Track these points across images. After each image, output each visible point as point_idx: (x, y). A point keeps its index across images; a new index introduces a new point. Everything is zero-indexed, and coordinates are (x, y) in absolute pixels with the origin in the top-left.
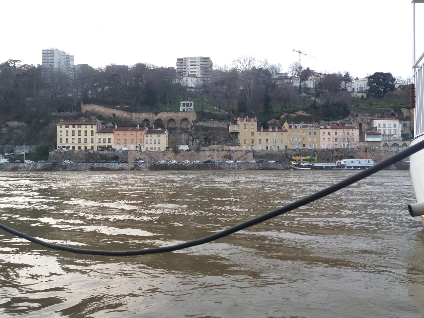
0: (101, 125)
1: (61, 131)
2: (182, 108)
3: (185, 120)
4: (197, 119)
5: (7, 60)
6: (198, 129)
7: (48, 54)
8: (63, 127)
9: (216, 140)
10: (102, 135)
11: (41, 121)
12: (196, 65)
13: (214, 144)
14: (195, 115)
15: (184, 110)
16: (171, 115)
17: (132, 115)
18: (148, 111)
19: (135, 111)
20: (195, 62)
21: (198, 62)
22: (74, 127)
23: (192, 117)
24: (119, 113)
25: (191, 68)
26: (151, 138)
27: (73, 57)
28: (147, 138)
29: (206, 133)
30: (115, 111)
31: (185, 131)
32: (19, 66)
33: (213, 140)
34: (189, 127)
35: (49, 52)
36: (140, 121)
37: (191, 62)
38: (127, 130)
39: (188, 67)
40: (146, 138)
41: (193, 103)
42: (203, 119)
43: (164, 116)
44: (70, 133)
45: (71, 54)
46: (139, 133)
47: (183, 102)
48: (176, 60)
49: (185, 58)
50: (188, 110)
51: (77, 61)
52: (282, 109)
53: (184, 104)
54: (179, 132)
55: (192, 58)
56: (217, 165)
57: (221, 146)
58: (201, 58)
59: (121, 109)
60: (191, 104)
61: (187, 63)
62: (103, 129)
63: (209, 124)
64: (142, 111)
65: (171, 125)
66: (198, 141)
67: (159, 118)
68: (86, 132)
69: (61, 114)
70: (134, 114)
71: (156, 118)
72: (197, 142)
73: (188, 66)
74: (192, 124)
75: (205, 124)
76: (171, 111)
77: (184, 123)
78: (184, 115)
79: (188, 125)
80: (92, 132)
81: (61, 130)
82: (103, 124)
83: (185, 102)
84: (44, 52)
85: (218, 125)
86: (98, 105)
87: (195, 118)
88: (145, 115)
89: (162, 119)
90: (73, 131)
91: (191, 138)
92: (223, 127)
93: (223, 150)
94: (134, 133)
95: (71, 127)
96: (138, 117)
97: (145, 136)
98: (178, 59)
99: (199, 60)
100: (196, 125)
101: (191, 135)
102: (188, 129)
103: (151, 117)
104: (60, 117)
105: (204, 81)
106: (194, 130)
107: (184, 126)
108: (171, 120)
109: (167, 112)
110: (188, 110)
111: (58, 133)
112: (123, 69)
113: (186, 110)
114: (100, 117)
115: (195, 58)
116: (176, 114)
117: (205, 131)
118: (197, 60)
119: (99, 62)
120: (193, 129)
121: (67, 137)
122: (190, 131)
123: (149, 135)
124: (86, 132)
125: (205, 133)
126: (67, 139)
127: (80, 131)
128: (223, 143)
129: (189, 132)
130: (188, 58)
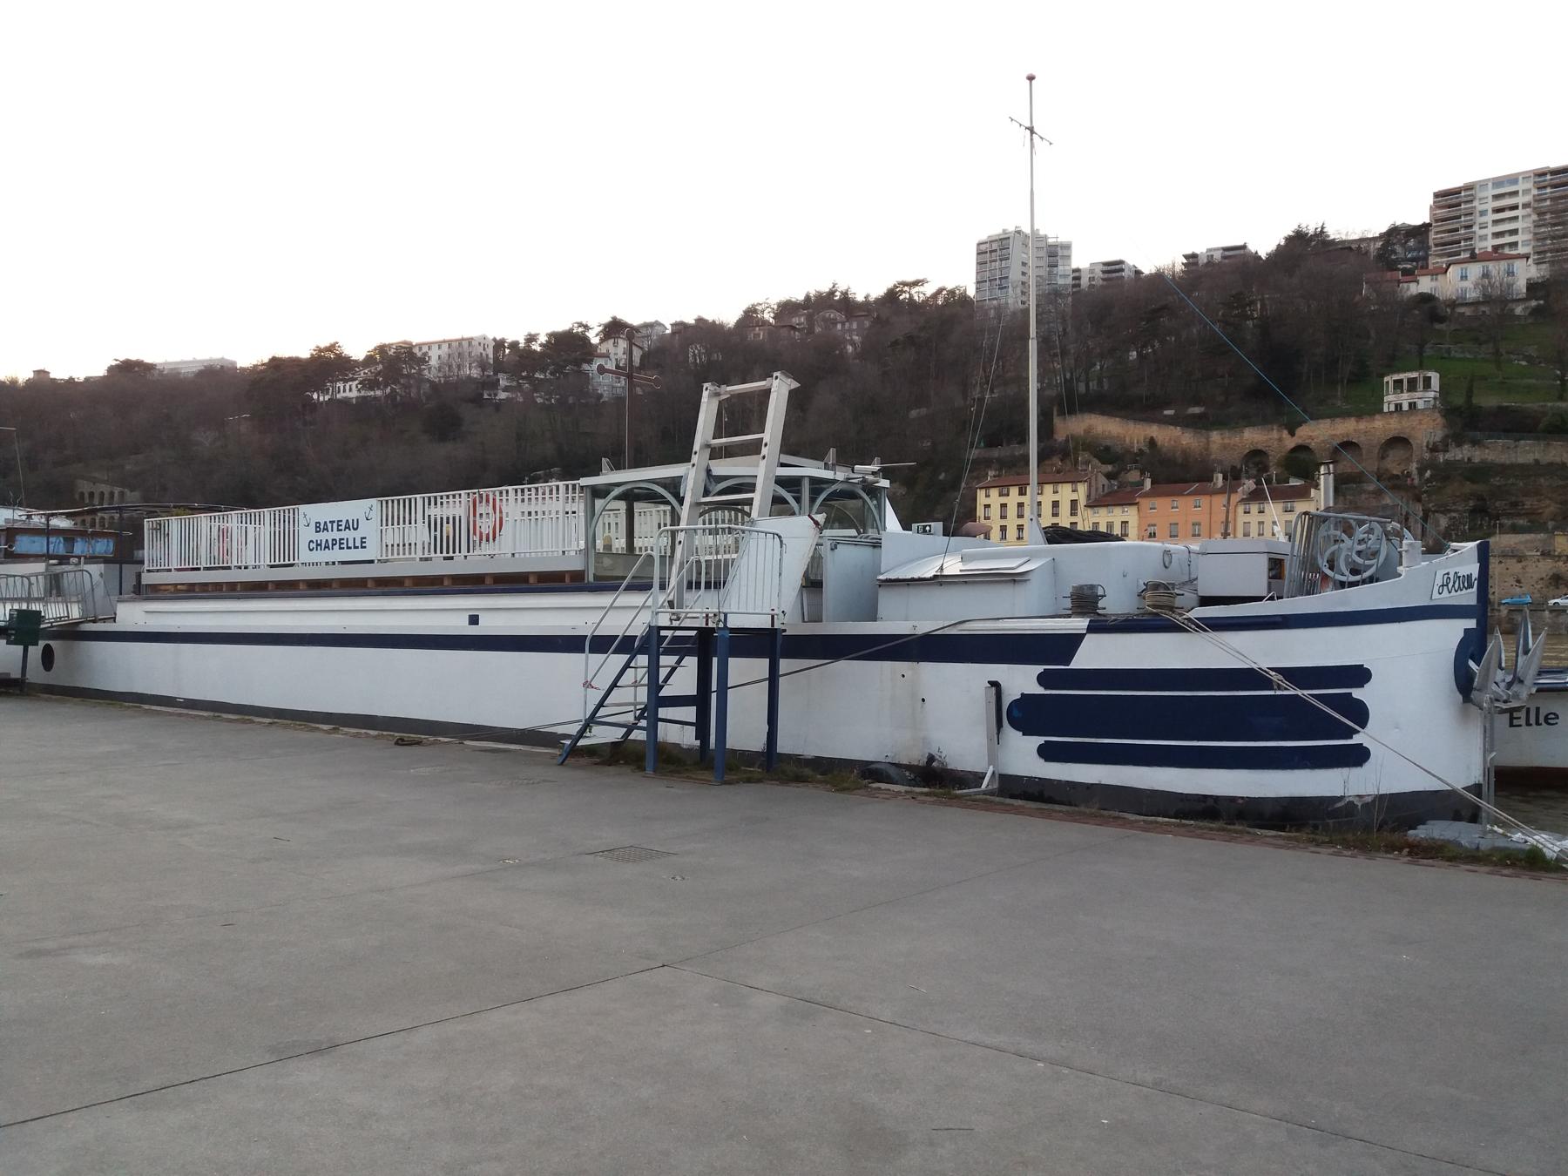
0: (1103, 480)
1: (987, 506)
2: (1390, 399)
3: (1399, 441)
4: (1447, 436)
5: (890, 285)
6: (1445, 474)
7: (994, 253)
8: (994, 492)
9: (1526, 514)
10: (1103, 511)
11: (942, 477)
12: (1515, 207)
13: (1515, 530)
14: (1440, 420)
15: (1398, 407)
16: (1346, 428)
17: (1208, 438)
18: (1264, 421)
19: (1221, 423)
20: (1515, 193)
21: (1526, 192)
22: (1022, 493)
23: (1427, 430)
24: (1170, 437)
25: (1495, 222)
26: (1261, 518)
27: (1067, 247)
28: (1247, 518)
29: (1479, 488)
30: (1154, 431)
31: (1397, 483)
32: (922, 297)
33: (1509, 516)
34: (1414, 467)
35: (995, 246)
36: (1235, 458)
37: (1496, 197)
38: (1181, 494)
39: (1483, 219)
40: (1242, 518)
41: (1435, 378)
42: (1471, 434)
43: (1318, 433)
44: (1012, 511)
45: (1062, 239)
46: (1220, 500)
47: (1396, 377)
48: (1430, 200)
49: (1469, 187)
50: (1412, 406)
51: (1086, 257)
52: (737, 540)
53: (1398, 383)
54: (1371, 487)
55: (1498, 182)
56: (1504, 612)
57: (1542, 536)
58: (1541, 174)
59: (1172, 421)
60: (1427, 381)
61: (1476, 203)
62: (1108, 494)
63: (1496, 452)
64: (1248, 421)
65: (1349, 464)
66: (1443, 522)
67: (1300, 442)
68: (1056, 504)
69: (996, 453)
70: (1215, 436)
71: (1290, 443)
72: (1437, 524)
73: (1483, 213)
74: (1427, 456)
75: (1477, 455)
76: (1345, 415)
77: (1395, 455)
78: (1393, 426)
79: (1409, 460)
80: (1074, 503)
81: (987, 501)
82: (1109, 476)
83: (1404, 376)
84: (983, 247)
85: (1537, 456)
86: (1103, 413)
87: (1439, 435)
88: (1252, 437)
89: (1313, 445)
90: (1021, 505)
91: (1419, 509)
92: (1558, 460)
93: (1546, 554)
94: (1204, 500)
95: (1014, 491)
96: (1226, 444)
97: (1241, 509)
98: (1436, 195)
99: (1529, 185)
100: (1441, 458)
101: (1419, 500)
102: (1409, 475)
103: (1271, 439)
104: (987, 463)
105: (1552, 263)
106: (1428, 481)
107: (1393, 465)
108: (1348, 445)
109: (1329, 417)
110: (1412, 406)
111: (980, 511)
112: (1237, 261)
113: (1405, 407)
114: (1107, 454)
115: (1513, 179)
116: (1363, 425)
117: (1473, 482)
118: (1520, 187)
119: (1156, 251)
120: (1428, 474)
121: (1003, 522)
122: (1416, 482)
123: (1254, 508)
124: (1056, 504)
125: (1475, 487)
126: (1003, 529)
127: (1004, 506)
128: (1550, 524)
129: (1413, 487)
130: (1483, 184)
